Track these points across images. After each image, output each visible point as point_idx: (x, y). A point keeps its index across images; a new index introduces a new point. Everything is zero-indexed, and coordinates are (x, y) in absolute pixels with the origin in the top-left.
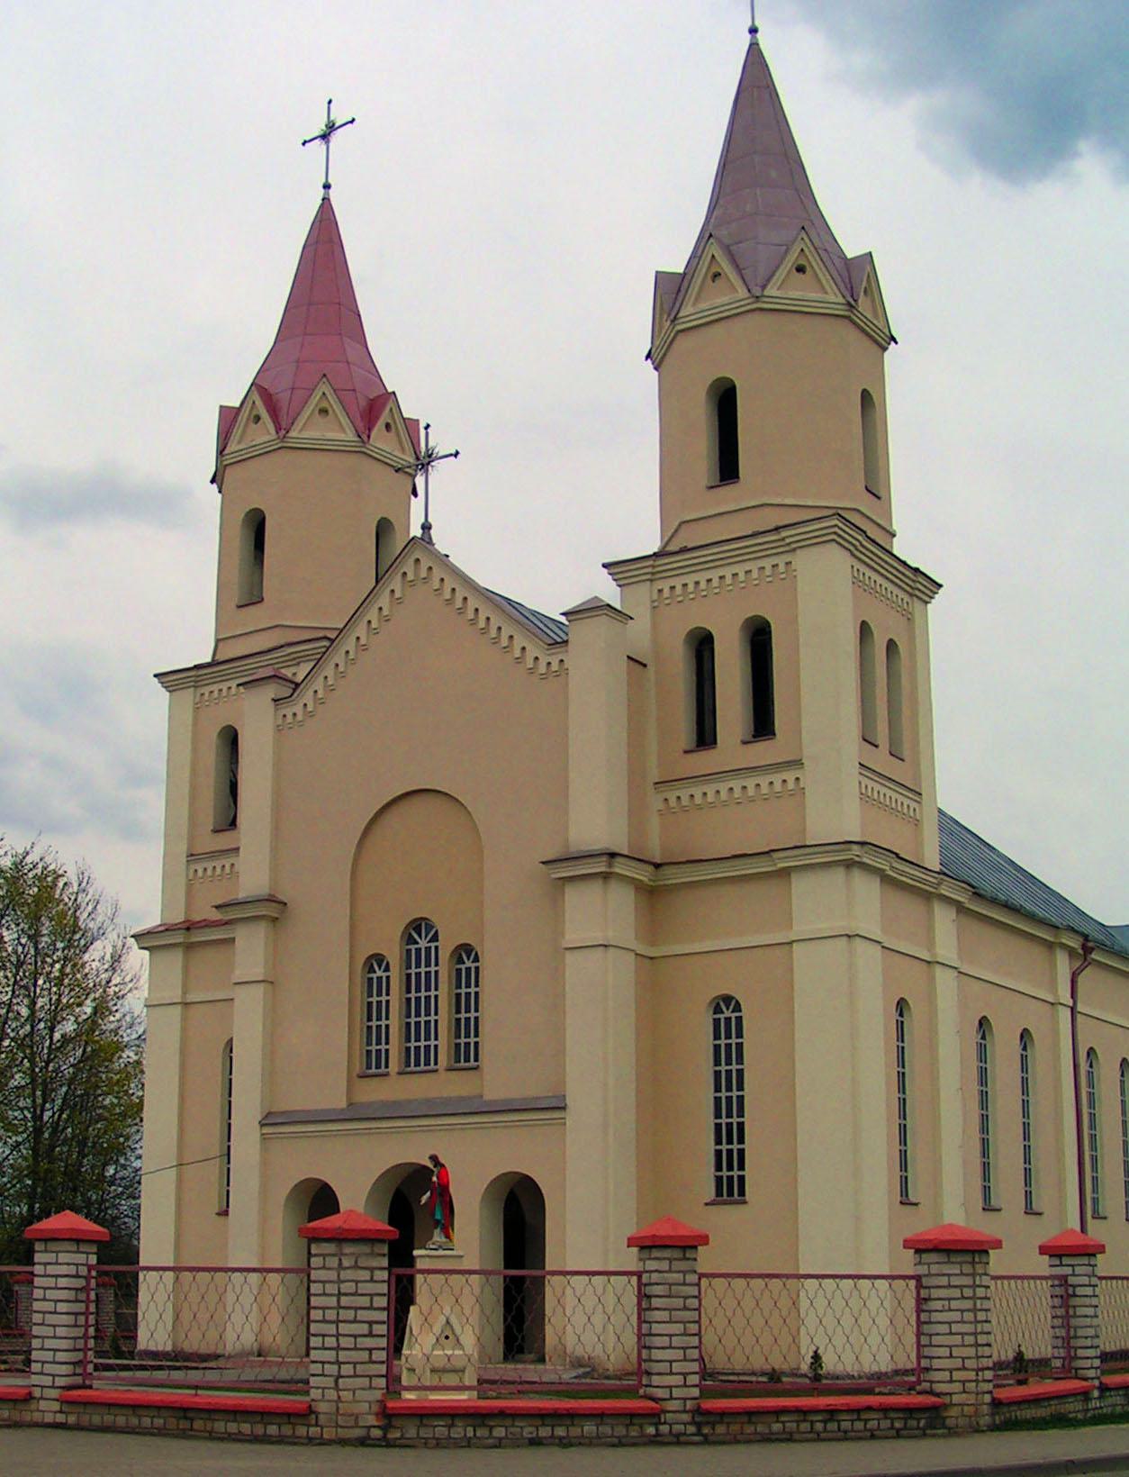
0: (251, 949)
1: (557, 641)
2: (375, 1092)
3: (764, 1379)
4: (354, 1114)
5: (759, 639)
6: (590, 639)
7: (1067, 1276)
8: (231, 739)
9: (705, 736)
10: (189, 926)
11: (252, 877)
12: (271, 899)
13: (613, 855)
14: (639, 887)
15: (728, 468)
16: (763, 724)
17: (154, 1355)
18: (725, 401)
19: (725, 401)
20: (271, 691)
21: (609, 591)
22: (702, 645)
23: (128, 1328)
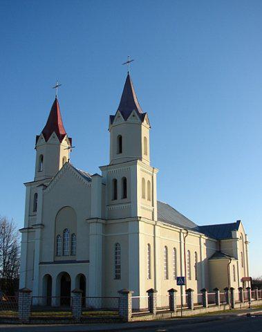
0: (38, 231)
1: (89, 180)
2: (58, 259)
3: (156, 171)
4: (55, 262)
5: (125, 180)
6: (95, 180)
7: (186, 285)
8: (36, 195)
9: (115, 198)
10: (29, 228)
11: (38, 221)
12: (41, 225)
13: (98, 218)
14: (103, 224)
15: (121, 152)
16: (125, 196)
17: (55, 307)
18: (120, 138)
19: (120, 138)
20: (42, 187)
21: (100, 173)
22: (115, 181)
23: (50, 303)
